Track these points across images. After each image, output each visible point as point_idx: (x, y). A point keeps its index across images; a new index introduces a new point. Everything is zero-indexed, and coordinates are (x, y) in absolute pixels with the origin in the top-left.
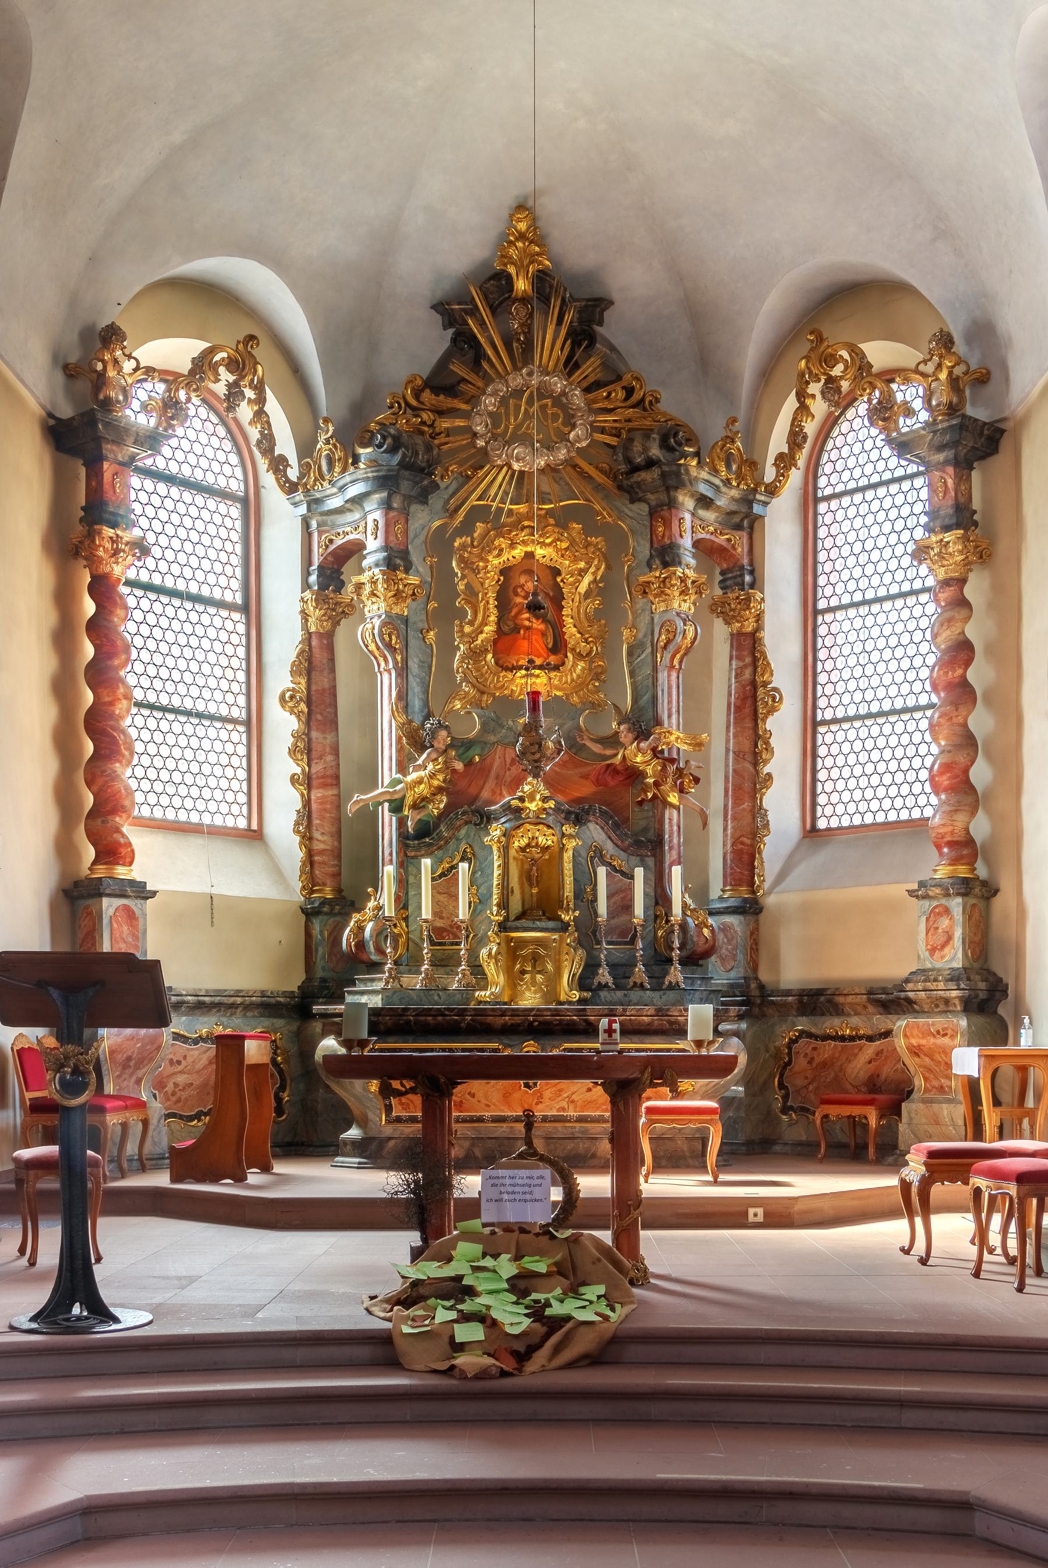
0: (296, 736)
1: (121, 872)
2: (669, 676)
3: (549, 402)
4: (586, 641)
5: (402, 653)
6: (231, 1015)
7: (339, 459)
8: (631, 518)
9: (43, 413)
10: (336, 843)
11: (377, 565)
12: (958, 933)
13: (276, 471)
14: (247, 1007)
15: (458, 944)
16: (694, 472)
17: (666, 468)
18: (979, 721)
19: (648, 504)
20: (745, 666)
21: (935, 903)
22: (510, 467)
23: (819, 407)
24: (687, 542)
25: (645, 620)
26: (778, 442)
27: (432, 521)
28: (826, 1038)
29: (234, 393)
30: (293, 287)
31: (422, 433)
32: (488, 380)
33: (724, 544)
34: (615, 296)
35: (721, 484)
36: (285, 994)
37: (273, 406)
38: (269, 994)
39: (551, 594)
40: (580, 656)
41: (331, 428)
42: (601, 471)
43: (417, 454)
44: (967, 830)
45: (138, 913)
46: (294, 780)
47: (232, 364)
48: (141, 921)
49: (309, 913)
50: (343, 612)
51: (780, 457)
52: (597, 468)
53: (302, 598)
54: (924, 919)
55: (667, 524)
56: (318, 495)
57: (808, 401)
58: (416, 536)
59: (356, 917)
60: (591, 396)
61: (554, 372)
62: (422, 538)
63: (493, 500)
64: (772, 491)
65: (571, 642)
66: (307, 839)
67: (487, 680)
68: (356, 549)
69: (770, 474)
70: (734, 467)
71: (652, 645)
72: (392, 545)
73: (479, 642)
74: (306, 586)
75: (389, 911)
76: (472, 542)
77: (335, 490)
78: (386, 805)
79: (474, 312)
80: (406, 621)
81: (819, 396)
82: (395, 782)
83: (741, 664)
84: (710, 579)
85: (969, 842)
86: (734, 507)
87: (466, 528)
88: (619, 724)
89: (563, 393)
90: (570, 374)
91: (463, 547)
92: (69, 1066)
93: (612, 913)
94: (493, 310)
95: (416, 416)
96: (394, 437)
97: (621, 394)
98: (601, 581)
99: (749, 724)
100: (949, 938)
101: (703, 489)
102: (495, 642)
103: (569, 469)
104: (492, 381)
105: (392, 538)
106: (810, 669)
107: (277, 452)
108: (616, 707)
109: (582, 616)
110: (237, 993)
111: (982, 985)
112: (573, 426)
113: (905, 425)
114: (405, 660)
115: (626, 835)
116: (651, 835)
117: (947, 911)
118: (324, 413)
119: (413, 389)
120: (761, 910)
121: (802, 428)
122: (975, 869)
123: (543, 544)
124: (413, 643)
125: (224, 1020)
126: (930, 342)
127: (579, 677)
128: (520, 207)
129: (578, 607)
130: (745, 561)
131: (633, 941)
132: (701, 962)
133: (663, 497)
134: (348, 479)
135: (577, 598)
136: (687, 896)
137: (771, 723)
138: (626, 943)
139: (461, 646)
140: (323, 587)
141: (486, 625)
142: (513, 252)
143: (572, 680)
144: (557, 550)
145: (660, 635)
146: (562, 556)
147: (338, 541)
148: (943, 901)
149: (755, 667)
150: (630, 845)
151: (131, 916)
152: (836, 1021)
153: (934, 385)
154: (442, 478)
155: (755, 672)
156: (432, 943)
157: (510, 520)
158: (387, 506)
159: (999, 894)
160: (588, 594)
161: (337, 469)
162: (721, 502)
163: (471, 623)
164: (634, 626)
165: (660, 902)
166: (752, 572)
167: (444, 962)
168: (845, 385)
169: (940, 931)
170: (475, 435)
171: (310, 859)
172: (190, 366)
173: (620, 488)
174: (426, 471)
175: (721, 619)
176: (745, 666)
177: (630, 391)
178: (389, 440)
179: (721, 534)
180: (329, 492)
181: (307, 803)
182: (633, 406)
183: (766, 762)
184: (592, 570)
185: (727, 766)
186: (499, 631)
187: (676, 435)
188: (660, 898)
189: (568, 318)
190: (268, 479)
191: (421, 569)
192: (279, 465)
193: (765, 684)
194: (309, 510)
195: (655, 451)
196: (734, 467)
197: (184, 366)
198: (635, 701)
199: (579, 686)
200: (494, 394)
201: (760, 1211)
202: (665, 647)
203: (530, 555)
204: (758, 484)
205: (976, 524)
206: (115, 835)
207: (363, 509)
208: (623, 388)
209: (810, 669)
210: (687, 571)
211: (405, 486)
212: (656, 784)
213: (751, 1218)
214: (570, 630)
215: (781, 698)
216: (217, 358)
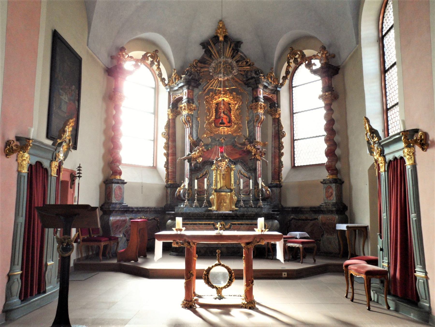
0: (166, 143)
1: (118, 177)
2: (257, 128)
3: (228, 65)
4: (237, 120)
5: (191, 123)
6: (146, 213)
7: (177, 78)
8: (248, 91)
9: (106, 67)
10: (175, 170)
11: (186, 102)
12: (334, 193)
13: (162, 81)
14: (150, 212)
15: (204, 195)
16: (263, 80)
17: (256, 79)
18: (337, 138)
19: (252, 87)
20: (276, 126)
21: (328, 185)
22: (218, 79)
23: (293, 65)
24: (261, 96)
25: (252, 115)
26: (283, 74)
27: (199, 92)
28: (299, 220)
29: (152, 63)
30: (167, 39)
31: (197, 73)
32: (213, 60)
33: (270, 97)
34: (243, 41)
35: (269, 83)
36: (160, 208)
37: (162, 66)
38: (156, 208)
39: (228, 109)
40: (235, 124)
41: (176, 72)
42: (241, 80)
43: (196, 76)
44: (335, 166)
45: (122, 188)
46: (165, 154)
47: (152, 57)
48: (123, 190)
49: (167, 187)
50: (178, 114)
51: (284, 77)
52: (239, 80)
53: (168, 111)
54: (325, 189)
55: (257, 92)
56: (172, 87)
57: (290, 64)
58: (195, 96)
59: (179, 188)
60: (238, 63)
61: (229, 58)
62: (197, 96)
63: (214, 87)
64: (282, 85)
65: (233, 121)
66: (167, 169)
67: (212, 130)
68: (181, 99)
69: (281, 81)
70: (272, 79)
71: (253, 121)
72: (189, 97)
73: (211, 121)
74: (169, 108)
75: (187, 187)
76: (209, 97)
77: (176, 85)
78: (187, 160)
79: (210, 45)
80: (192, 115)
81: (293, 62)
82: (189, 155)
83: (275, 126)
84: (267, 105)
85: (336, 169)
86: (272, 88)
87: (208, 94)
88: (245, 140)
89: (231, 63)
90: (232, 59)
91: (207, 98)
92: (65, 243)
93: (244, 188)
94: (214, 44)
95: (196, 69)
96: (190, 73)
97: (245, 63)
98: (240, 106)
99: (277, 140)
100: (332, 194)
101: (265, 84)
102: (215, 121)
103: (232, 80)
104: (214, 60)
105: (189, 96)
106: (292, 127)
107: (163, 77)
108: (244, 136)
109: (236, 114)
110: (148, 208)
111: (341, 207)
112: (234, 70)
113: (314, 68)
114: (192, 125)
115: (247, 167)
116: (254, 167)
117: (331, 187)
118: (174, 68)
119: (195, 63)
120: (281, 186)
121: (289, 70)
122: (338, 176)
123: (226, 97)
124: (194, 121)
125: (145, 215)
126: (320, 48)
127: (235, 129)
128: (221, 21)
129: (235, 112)
130: (276, 101)
131: (249, 195)
132: (267, 200)
133: (256, 86)
134: (179, 82)
135: (235, 110)
136: (263, 183)
137: (283, 140)
138: (247, 195)
139: (206, 122)
140: (173, 108)
141: (212, 116)
142: (219, 31)
143: (234, 130)
144: (230, 99)
145: (255, 118)
146: (231, 100)
147: (177, 97)
148: (330, 184)
149: (279, 126)
150: (248, 170)
151: (120, 188)
152: (302, 215)
153: (321, 58)
154: (202, 82)
155: (279, 128)
156: (198, 195)
157: (218, 92)
158: (188, 89)
159: (344, 183)
160: (237, 109)
161: (177, 80)
162: (270, 87)
163: (209, 116)
164: (249, 116)
165: (256, 184)
166: (277, 104)
167: (200, 201)
168: (299, 60)
169: (329, 192)
170: (210, 72)
171: (168, 174)
172: (142, 57)
173: (245, 84)
174: (197, 81)
175: (270, 115)
176: (276, 126)
177: (247, 62)
178: (189, 73)
179: (270, 95)
180: (175, 86)
181: (168, 160)
182: (248, 66)
183: (282, 149)
184: (238, 103)
185: (272, 150)
186: (216, 118)
187: (258, 71)
188: (256, 184)
189: (232, 46)
190: (161, 83)
191: (196, 103)
192: (163, 80)
193: (281, 130)
194: (170, 90)
195: (254, 75)
196: (272, 79)
197: (141, 57)
198: (249, 134)
199: (235, 131)
200: (215, 63)
201: (286, 273)
202: (256, 121)
203: (223, 100)
204: (278, 83)
205: (334, 91)
206: (117, 168)
207: (183, 89)
208: (245, 61)
209: (292, 127)
210: (262, 103)
211: (193, 84)
212: (255, 155)
213: (283, 276)
214: (233, 117)
215: (285, 134)
216: (148, 55)
